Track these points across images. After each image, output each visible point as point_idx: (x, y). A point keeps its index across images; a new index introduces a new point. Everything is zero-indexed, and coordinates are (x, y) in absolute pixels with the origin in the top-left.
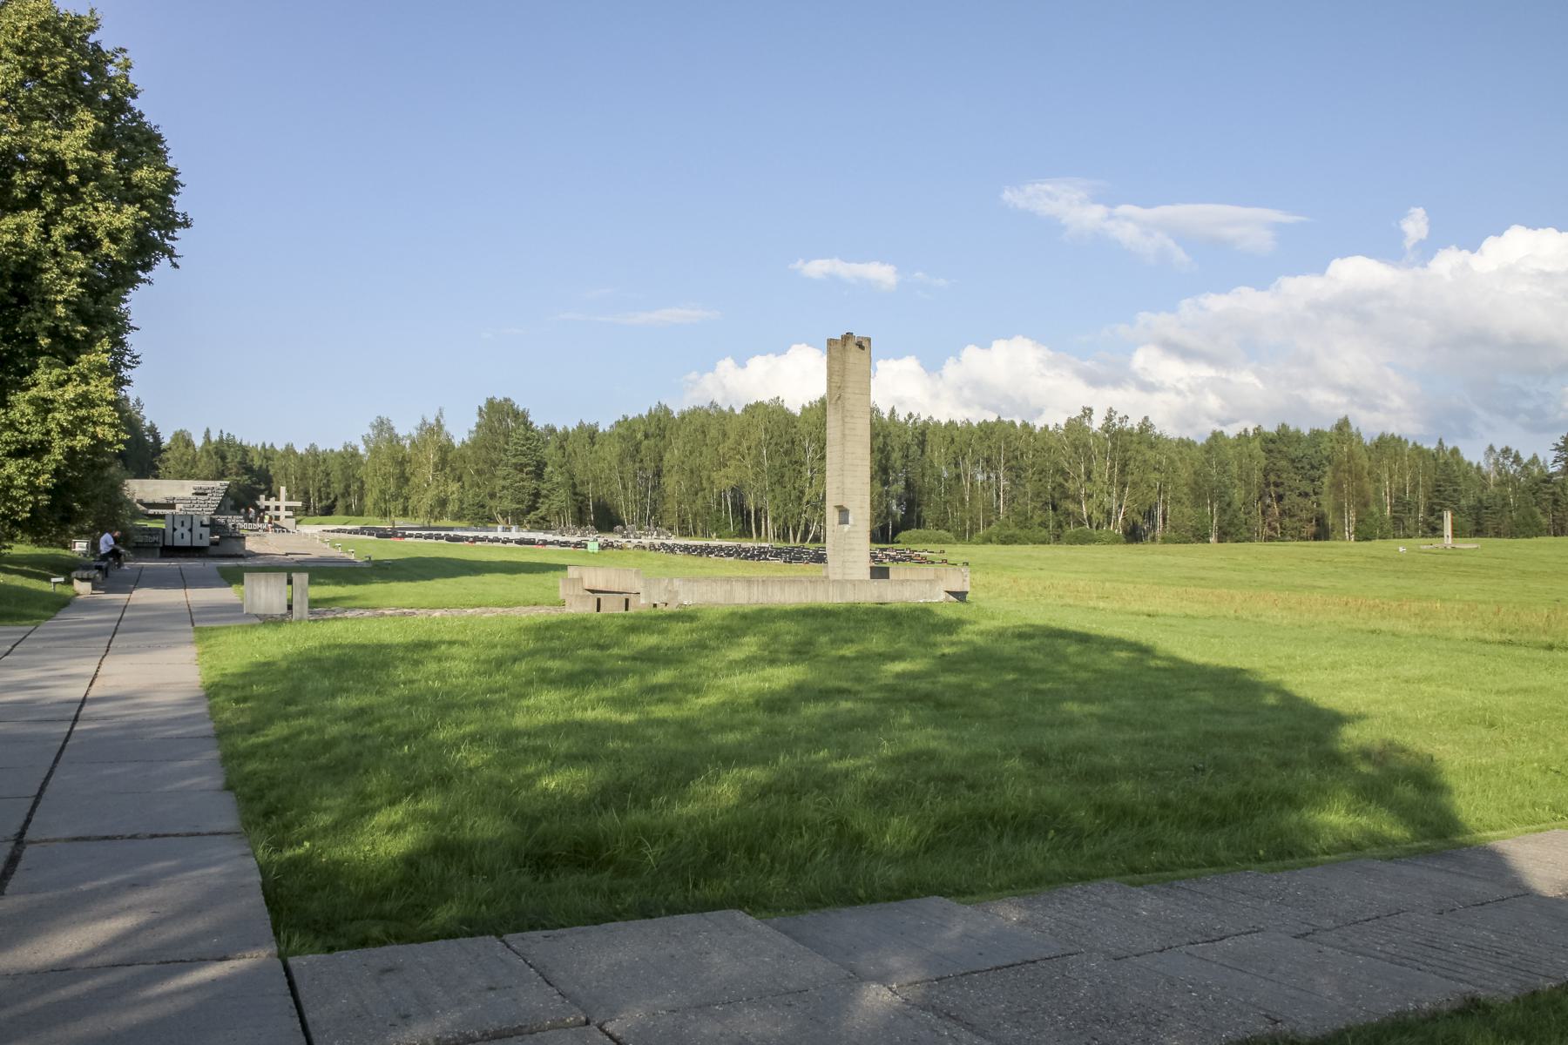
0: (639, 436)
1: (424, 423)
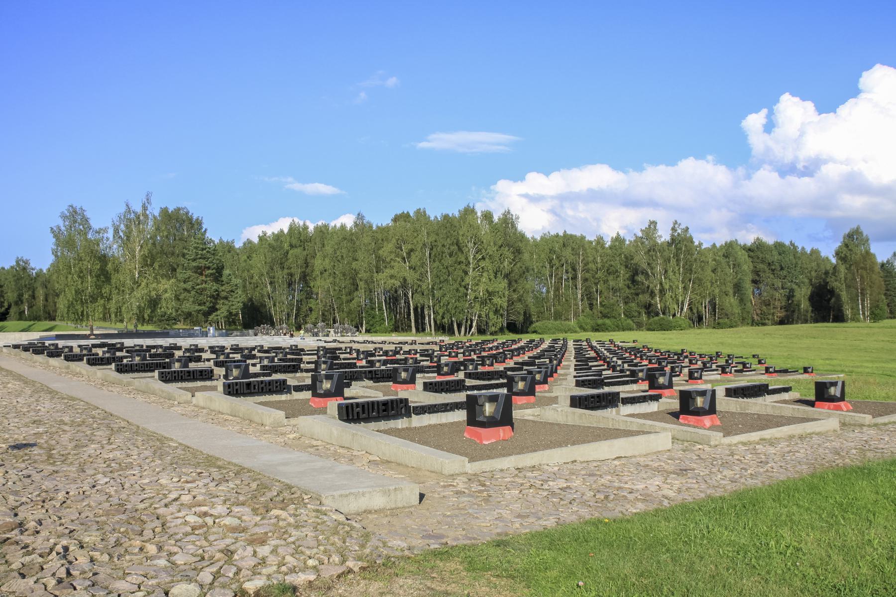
0: (286, 246)
1: (129, 210)
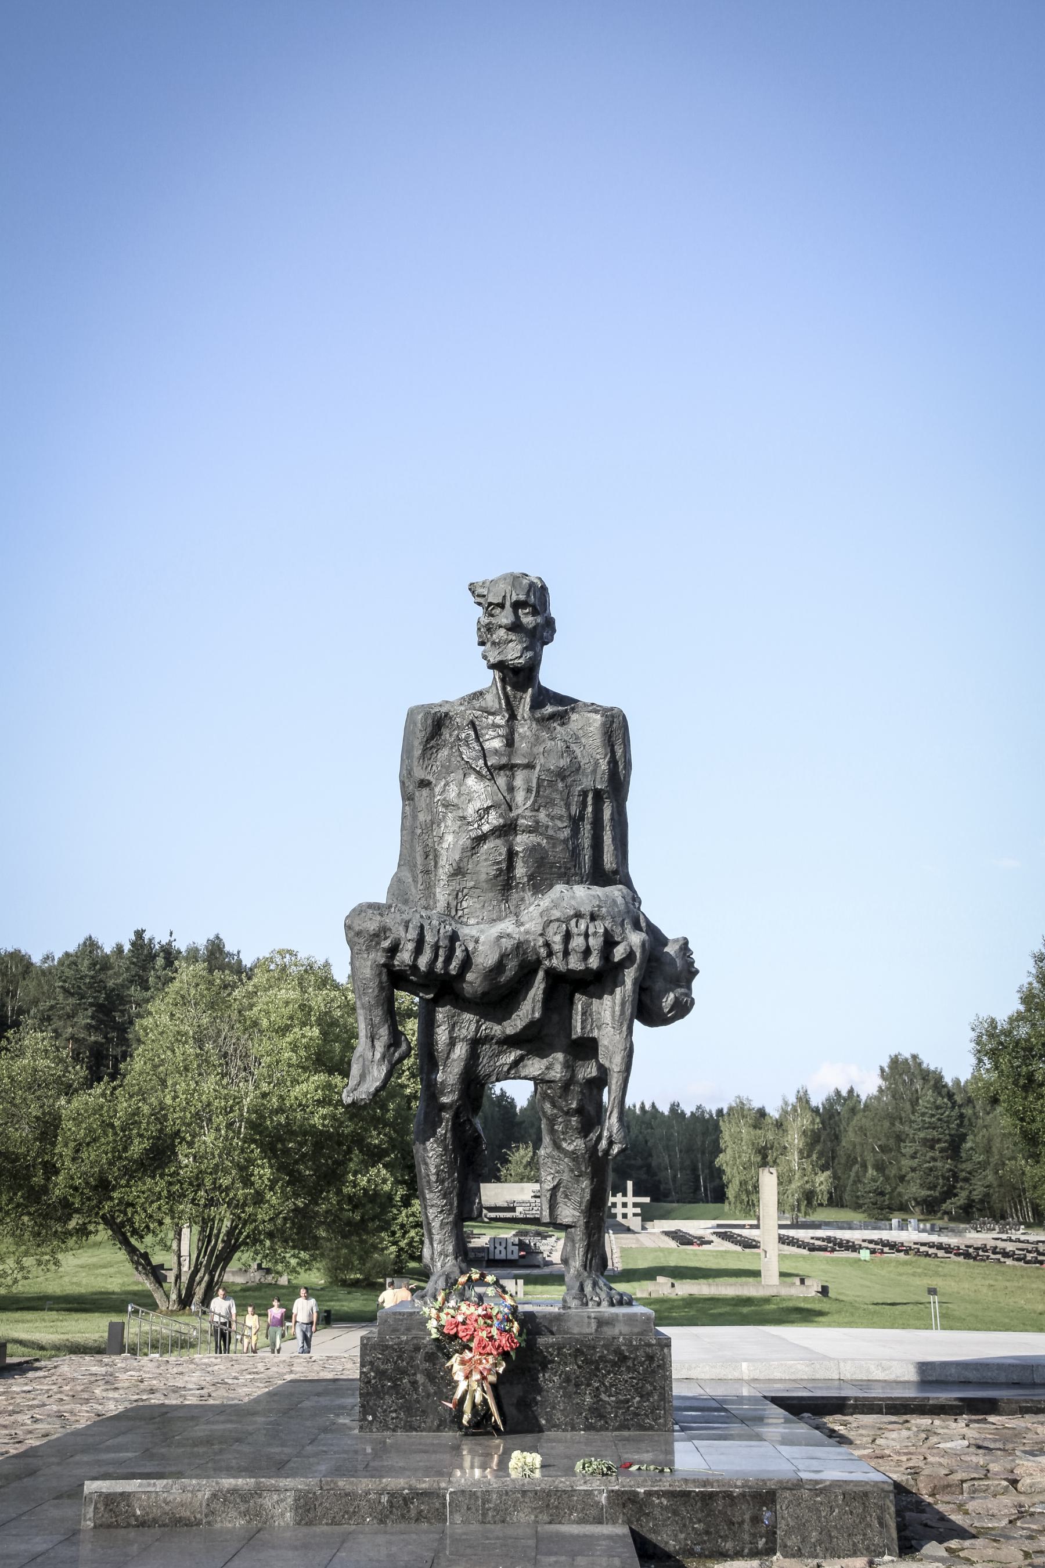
1: (786, 1104)
